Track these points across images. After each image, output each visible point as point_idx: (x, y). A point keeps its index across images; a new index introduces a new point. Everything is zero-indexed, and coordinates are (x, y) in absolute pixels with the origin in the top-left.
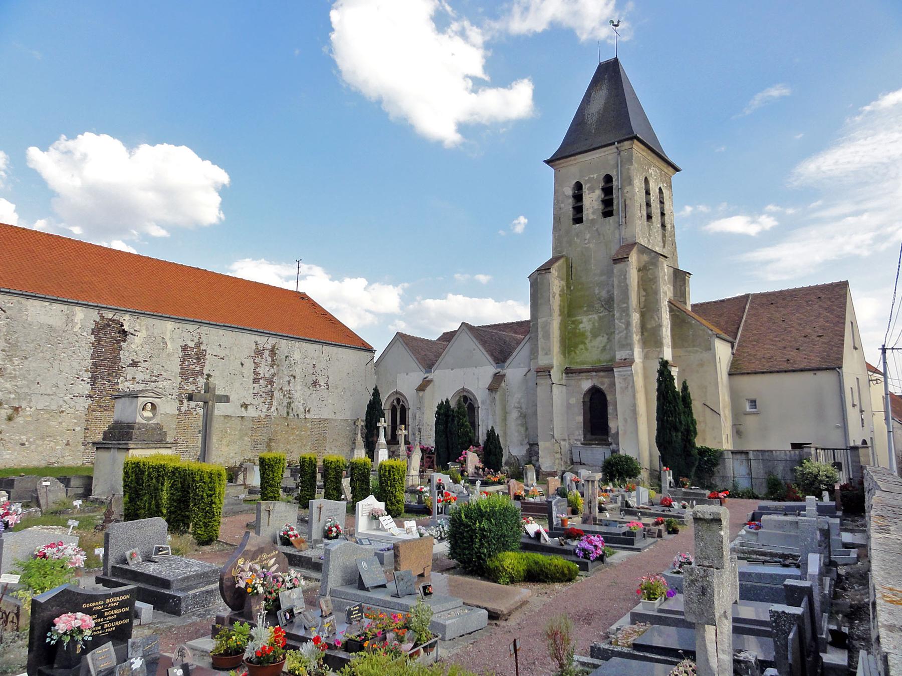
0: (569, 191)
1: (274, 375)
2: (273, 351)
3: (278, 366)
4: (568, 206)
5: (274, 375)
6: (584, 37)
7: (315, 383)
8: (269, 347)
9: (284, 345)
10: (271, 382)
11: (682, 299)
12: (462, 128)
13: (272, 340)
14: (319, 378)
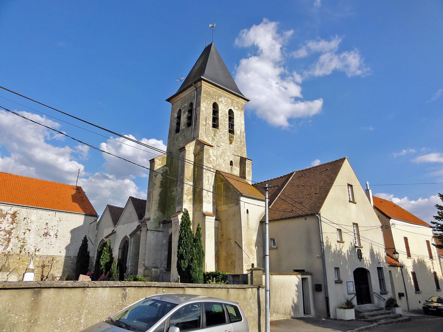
0: (176, 115)
1: (12, 229)
2: (14, 215)
3: (17, 223)
4: (175, 125)
5: (12, 229)
6: (350, 75)
7: (46, 234)
8: (12, 212)
9: (23, 212)
10: (10, 233)
11: (244, 176)
12: (290, 120)
13: (15, 209)
14: (49, 231)
